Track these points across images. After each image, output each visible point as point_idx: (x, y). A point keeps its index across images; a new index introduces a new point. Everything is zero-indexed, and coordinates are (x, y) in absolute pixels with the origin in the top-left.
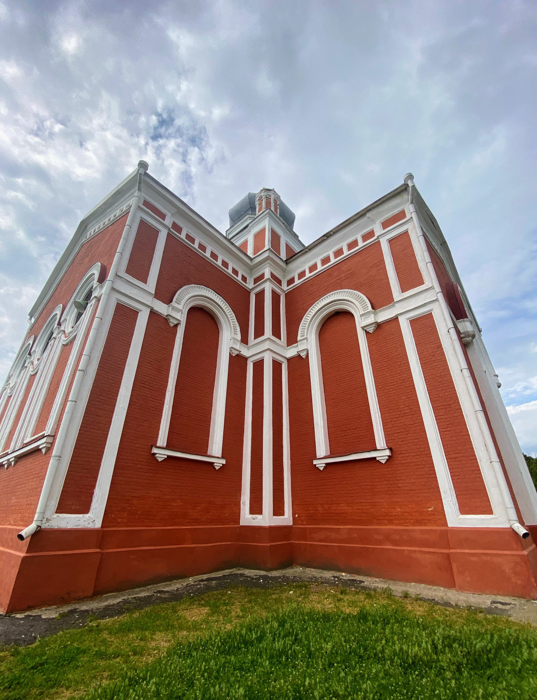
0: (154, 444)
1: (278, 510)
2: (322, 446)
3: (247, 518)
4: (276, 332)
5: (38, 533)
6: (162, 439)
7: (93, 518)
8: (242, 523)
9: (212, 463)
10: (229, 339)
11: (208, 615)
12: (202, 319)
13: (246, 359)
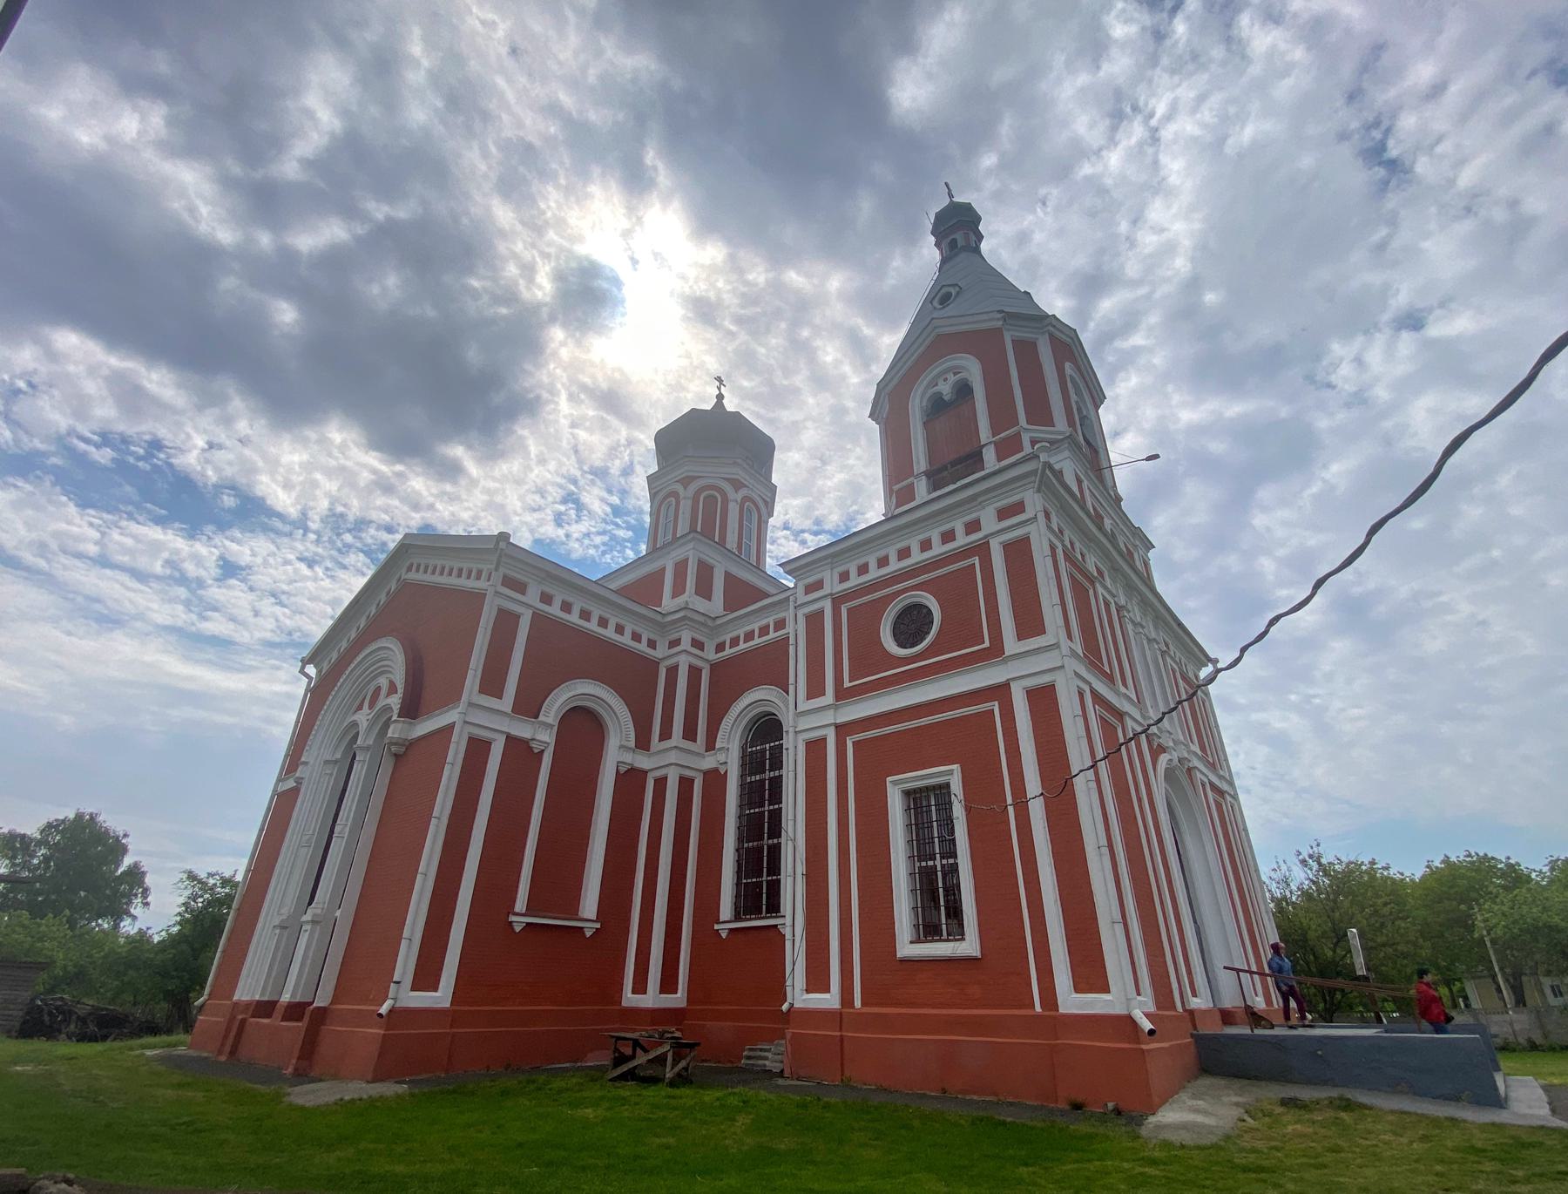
0: (510, 910)
1: (668, 985)
2: (726, 909)
3: (630, 999)
4: (690, 733)
6: (521, 904)
7: (441, 997)
8: (624, 1003)
10: (617, 752)
11: (558, 187)
12: (583, 728)
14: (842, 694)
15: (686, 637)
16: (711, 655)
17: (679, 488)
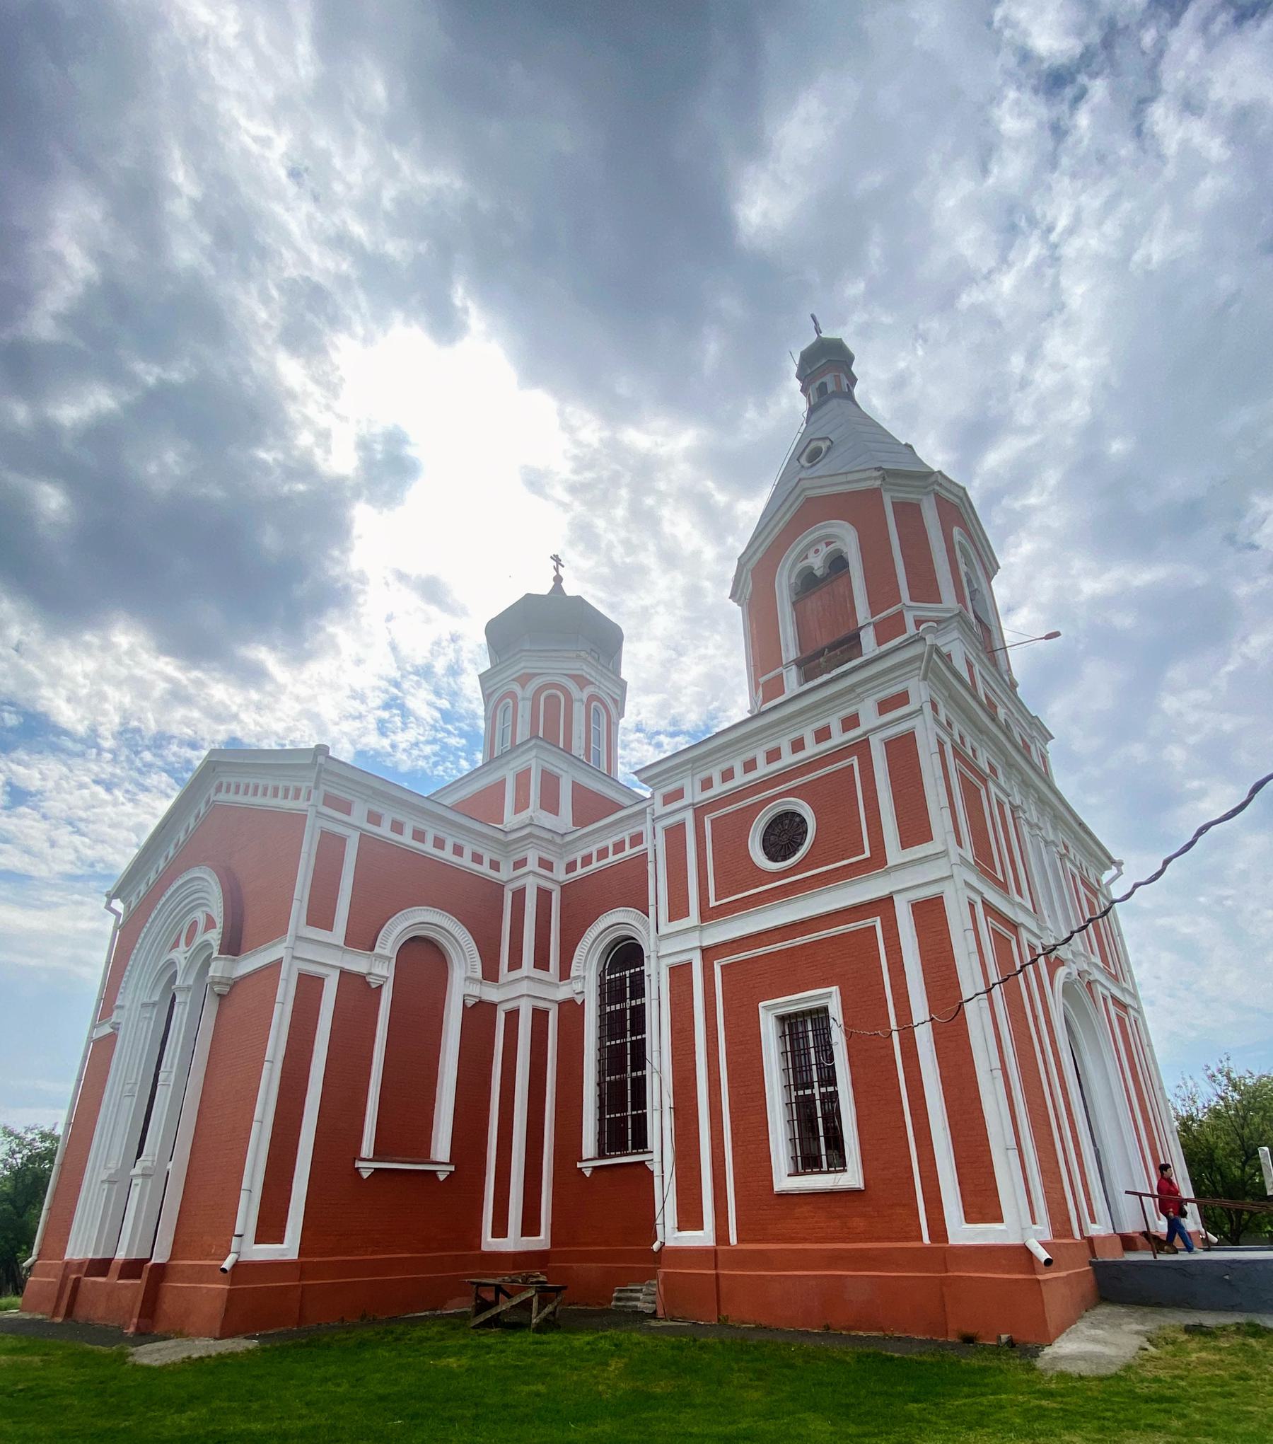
2: (589, 1145)
3: (489, 1243)
4: (541, 962)
5: (237, 1265)
6: (367, 1148)
9: (434, 1172)
10: (463, 984)
12: (423, 959)
13: (493, 1006)
14: (708, 915)
15: (533, 858)
16: (561, 875)
17: (516, 687)
